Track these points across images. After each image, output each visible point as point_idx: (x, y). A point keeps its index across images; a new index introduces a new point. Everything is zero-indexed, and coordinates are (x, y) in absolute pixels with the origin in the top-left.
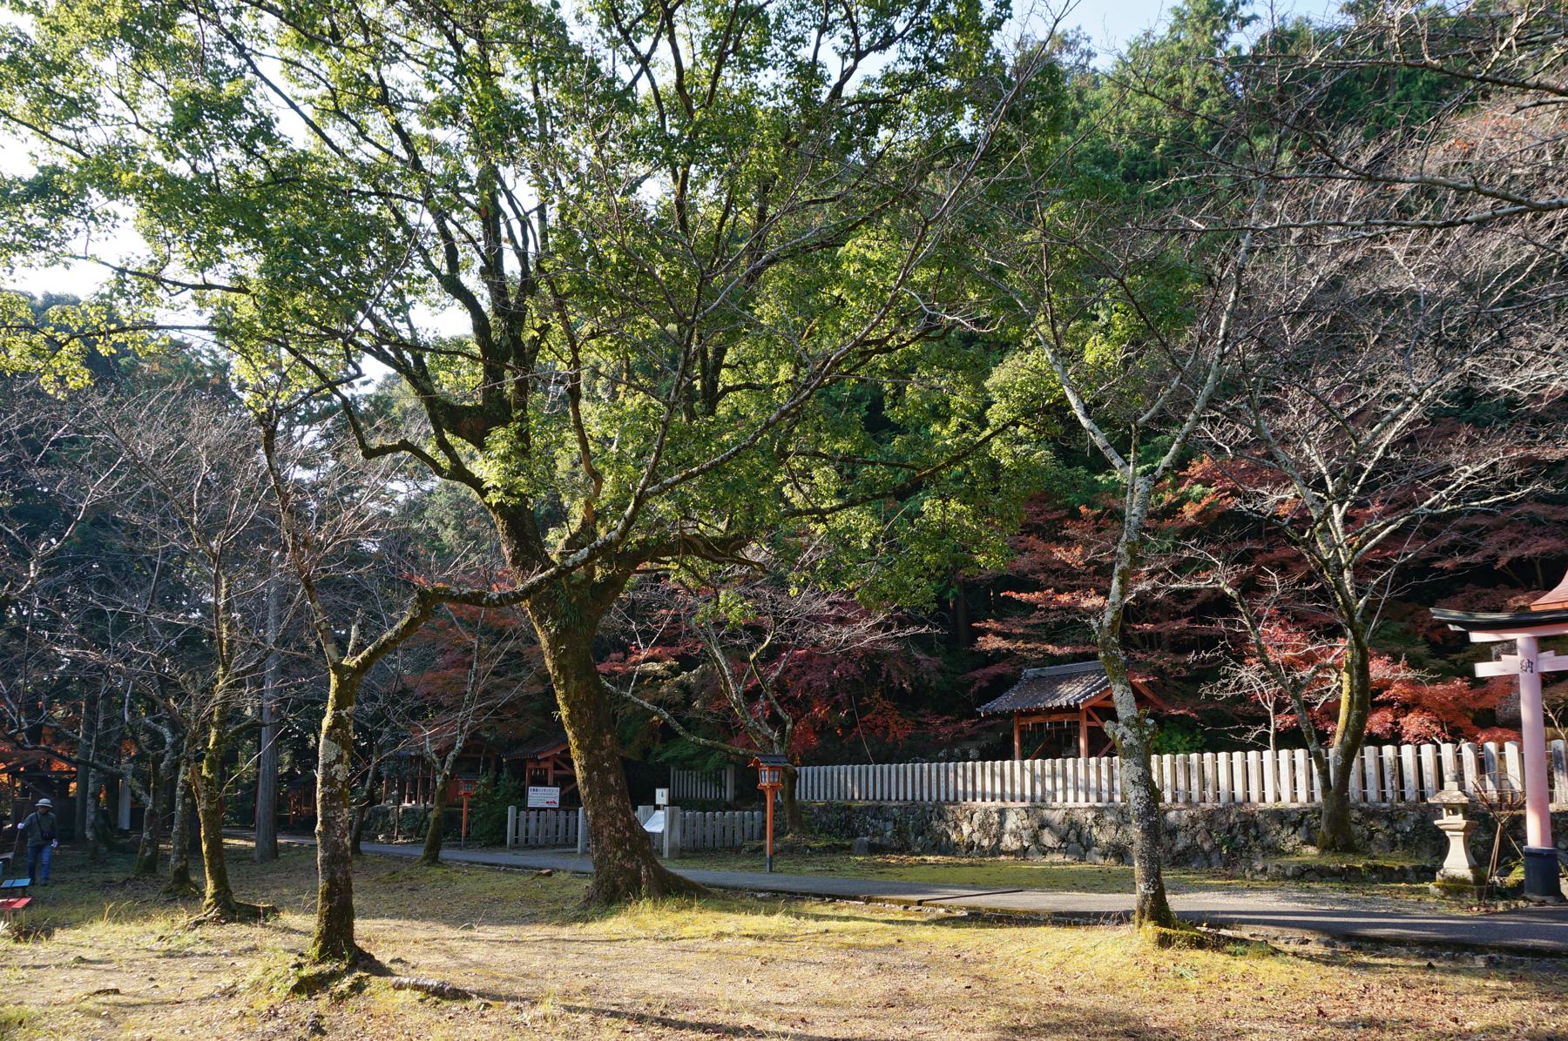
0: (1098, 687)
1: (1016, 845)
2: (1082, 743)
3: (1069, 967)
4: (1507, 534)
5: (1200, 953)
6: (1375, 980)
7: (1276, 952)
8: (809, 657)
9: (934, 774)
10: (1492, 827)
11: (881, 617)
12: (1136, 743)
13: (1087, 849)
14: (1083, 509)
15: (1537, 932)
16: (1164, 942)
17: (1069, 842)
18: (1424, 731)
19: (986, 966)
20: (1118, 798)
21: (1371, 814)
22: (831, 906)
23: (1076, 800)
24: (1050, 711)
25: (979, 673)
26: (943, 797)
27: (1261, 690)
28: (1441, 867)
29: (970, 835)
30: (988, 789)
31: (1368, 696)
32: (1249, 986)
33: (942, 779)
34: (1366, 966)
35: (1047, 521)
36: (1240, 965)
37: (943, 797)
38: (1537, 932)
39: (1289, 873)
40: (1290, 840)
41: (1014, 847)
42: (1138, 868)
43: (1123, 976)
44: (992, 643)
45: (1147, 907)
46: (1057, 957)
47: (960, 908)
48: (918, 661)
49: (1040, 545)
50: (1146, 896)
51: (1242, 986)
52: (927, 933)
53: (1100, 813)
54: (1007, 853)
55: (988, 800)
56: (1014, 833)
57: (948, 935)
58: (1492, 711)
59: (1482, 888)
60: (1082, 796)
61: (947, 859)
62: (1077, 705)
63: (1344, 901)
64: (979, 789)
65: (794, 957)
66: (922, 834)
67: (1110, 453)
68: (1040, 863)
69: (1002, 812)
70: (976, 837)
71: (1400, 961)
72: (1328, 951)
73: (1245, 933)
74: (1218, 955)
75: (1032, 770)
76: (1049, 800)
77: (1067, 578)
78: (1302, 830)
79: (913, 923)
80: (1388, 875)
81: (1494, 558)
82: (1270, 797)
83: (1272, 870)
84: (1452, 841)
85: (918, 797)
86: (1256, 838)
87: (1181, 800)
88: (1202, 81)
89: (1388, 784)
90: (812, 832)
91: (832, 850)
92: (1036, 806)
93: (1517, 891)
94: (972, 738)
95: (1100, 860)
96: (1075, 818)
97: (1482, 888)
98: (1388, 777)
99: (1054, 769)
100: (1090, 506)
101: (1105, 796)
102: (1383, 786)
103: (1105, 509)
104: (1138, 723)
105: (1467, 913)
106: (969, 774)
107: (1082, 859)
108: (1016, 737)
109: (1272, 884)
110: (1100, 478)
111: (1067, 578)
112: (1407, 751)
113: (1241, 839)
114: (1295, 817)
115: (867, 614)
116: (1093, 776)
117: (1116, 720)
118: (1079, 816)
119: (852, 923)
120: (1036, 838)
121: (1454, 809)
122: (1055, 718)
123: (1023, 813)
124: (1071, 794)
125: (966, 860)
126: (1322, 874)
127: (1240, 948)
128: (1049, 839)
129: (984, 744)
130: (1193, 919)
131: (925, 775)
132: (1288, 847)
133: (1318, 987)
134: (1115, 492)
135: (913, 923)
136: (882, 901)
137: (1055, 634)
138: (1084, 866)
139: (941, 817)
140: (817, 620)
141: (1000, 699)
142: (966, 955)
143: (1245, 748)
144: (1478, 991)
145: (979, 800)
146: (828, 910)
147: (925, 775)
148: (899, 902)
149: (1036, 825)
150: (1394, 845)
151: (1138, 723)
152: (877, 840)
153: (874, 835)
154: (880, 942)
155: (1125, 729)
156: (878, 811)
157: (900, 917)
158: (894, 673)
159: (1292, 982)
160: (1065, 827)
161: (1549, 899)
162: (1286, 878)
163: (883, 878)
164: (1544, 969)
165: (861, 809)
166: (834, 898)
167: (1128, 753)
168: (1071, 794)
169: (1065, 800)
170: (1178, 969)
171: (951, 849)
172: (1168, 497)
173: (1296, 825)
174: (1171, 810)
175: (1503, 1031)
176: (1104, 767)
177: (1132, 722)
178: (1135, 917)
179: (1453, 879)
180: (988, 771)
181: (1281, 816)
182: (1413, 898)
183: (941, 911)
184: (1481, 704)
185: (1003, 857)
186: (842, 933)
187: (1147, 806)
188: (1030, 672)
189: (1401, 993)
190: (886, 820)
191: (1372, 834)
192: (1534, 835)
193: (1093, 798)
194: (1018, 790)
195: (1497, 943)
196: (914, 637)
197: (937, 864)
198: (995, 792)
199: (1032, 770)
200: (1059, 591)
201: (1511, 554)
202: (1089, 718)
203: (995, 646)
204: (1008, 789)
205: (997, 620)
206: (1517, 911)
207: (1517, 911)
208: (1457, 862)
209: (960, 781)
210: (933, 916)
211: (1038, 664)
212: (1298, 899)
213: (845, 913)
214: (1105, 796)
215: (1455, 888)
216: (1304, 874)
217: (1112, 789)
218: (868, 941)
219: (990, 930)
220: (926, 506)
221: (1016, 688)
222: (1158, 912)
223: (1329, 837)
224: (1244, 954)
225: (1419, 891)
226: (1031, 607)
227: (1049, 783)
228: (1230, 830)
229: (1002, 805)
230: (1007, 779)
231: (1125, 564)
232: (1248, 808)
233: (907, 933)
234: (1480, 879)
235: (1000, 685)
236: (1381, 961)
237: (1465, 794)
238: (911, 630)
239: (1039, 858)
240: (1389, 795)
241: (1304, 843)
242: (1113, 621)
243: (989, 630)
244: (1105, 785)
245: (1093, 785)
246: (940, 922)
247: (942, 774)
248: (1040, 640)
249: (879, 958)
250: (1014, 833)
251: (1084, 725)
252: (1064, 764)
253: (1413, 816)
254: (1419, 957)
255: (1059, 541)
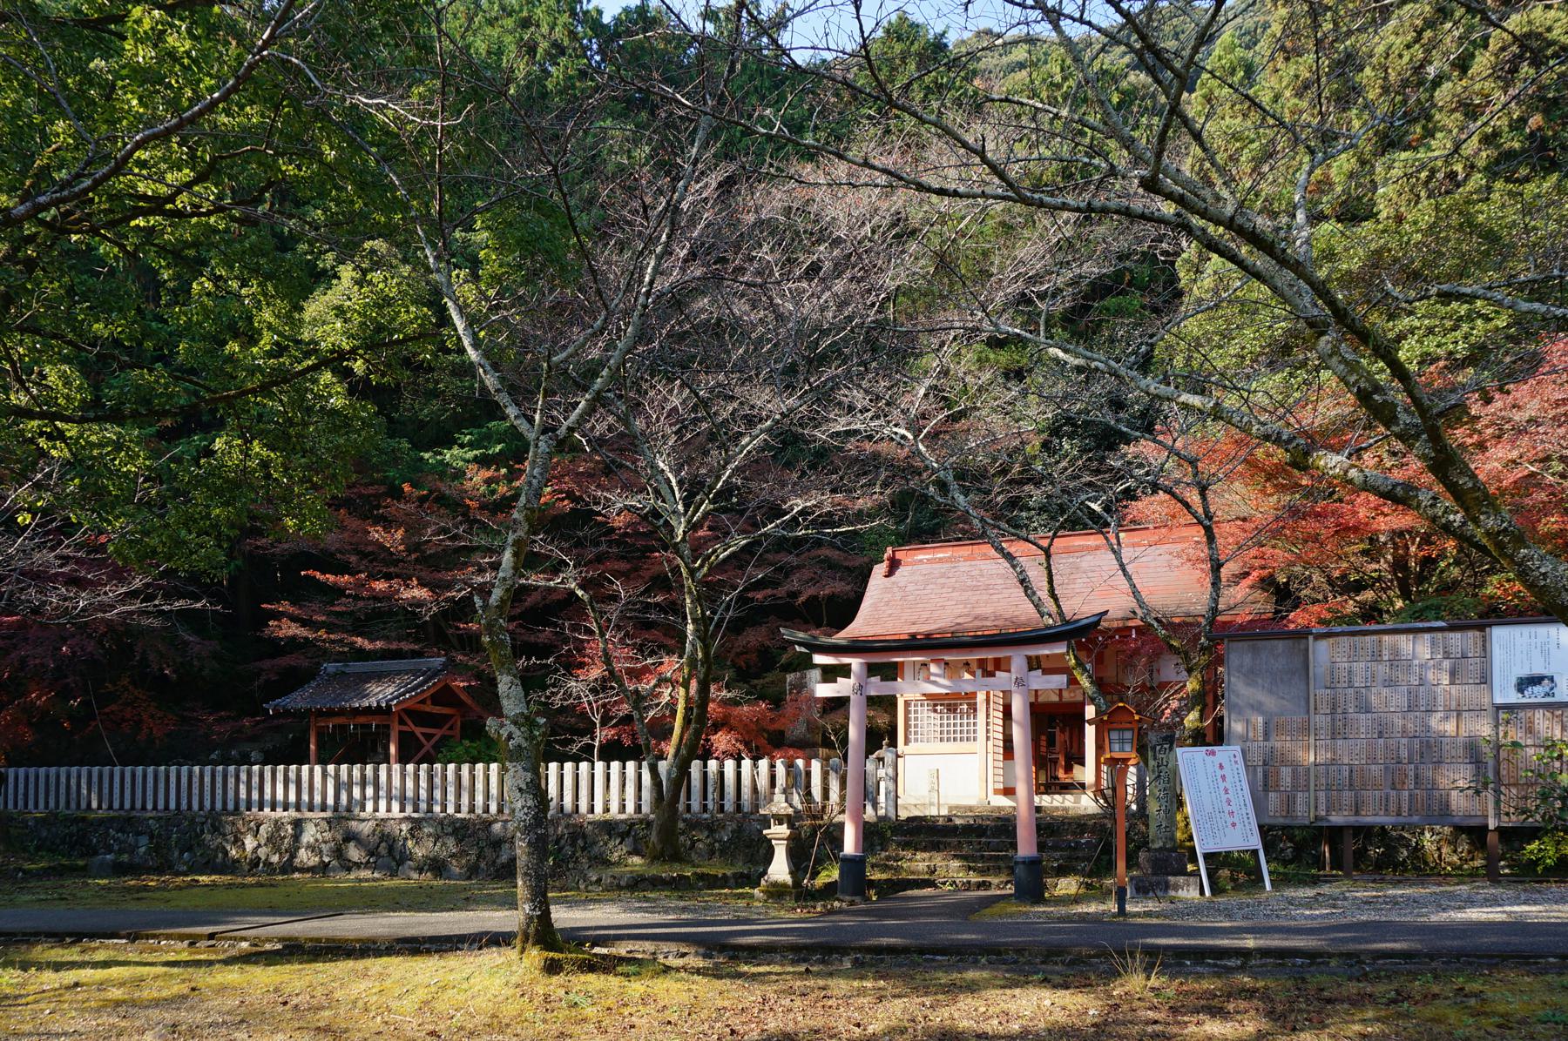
0: (413, 689)
1: (314, 861)
2: (393, 749)
3: (440, 1006)
4: (807, 574)
5: (591, 977)
6: (770, 991)
7: (667, 969)
8: (22, 626)
9: (207, 779)
10: (815, 838)
11: (137, 583)
12: (525, 745)
13: (400, 863)
14: (406, 487)
15: (888, 931)
16: (552, 968)
17: (379, 856)
18: (730, 748)
19: (327, 1013)
20: (437, 809)
21: (694, 825)
22: (77, 949)
23: (389, 810)
24: (356, 712)
25: (266, 664)
26: (219, 806)
27: (590, 703)
28: (765, 873)
29: (255, 850)
30: (280, 796)
31: (698, 714)
32: (651, 1009)
33: (219, 785)
34: (753, 977)
35: (361, 496)
36: (637, 987)
37: (219, 806)
38: (888, 931)
39: (623, 883)
40: (617, 851)
41: (311, 863)
42: (521, 887)
43: (510, 1010)
44: (290, 629)
45: (532, 930)
46: (421, 994)
47: (269, 940)
48: (187, 643)
49: (354, 523)
50: (531, 918)
51: (643, 1010)
52: (232, 975)
53: (416, 824)
54: (302, 870)
55: (279, 810)
56: (311, 848)
57: (263, 976)
58: (782, 733)
59: (798, 893)
60: (396, 806)
61: (227, 879)
62: (389, 707)
63: (684, 909)
64: (267, 796)
65: (27, 1028)
66: (190, 849)
67: (503, 399)
68: (345, 880)
69: (298, 824)
70: (262, 852)
71: (777, 969)
72: (708, 963)
73: (622, 950)
74: (611, 978)
75: (337, 776)
76: (357, 810)
77: (382, 562)
78: (629, 841)
79: (210, 963)
80: (713, 882)
81: (794, 595)
82: (599, 808)
83: (607, 880)
84: (777, 850)
85: (184, 806)
86: (583, 849)
87: (506, 811)
88: (559, 33)
89: (710, 797)
90: (25, 850)
91: (59, 872)
92: (340, 817)
93: (830, 890)
94: (253, 739)
95: (415, 875)
96: (387, 830)
97: (798, 893)
98: (710, 789)
99: (363, 777)
100: (414, 485)
101: (423, 806)
102: (705, 798)
103: (431, 492)
104: (527, 721)
105: (791, 917)
106: (255, 780)
107: (394, 874)
108: (313, 740)
109: (608, 895)
110: (426, 456)
111: (382, 562)
112: (713, 765)
113: (568, 850)
114: (623, 828)
115: (119, 575)
116: (410, 784)
117: (500, 715)
118: (393, 828)
119: (115, 972)
120: (339, 853)
121: (780, 819)
122: (362, 720)
123: (324, 825)
124: (383, 804)
125: (249, 880)
126: (656, 883)
127: (632, 969)
128: (354, 853)
129: (269, 746)
130: (577, 938)
131: (196, 780)
132: (615, 857)
133: (720, 1004)
134: (442, 475)
135: (210, 963)
136: (154, 936)
137: (360, 625)
138: (396, 882)
139: (216, 829)
140: (40, 577)
141: (294, 695)
142: (295, 1001)
143: (577, 760)
144: (862, 992)
145: (267, 810)
146: (72, 954)
147: (196, 780)
148: (181, 938)
149: (339, 837)
150: (712, 853)
151: (527, 721)
152: (125, 857)
153: (121, 851)
154: (165, 993)
155: (513, 728)
156: (128, 823)
157: (184, 956)
158: (152, 657)
159: (693, 1001)
160: (374, 840)
161: (857, 899)
162: (620, 888)
163: (142, 906)
164: (901, 966)
165: (101, 821)
166: (77, 937)
167: (516, 755)
168: (383, 804)
169: (376, 810)
170: (571, 996)
171: (231, 867)
172: (502, 489)
173: (623, 837)
174: (496, 821)
175: (903, 1031)
176: (423, 774)
177: (522, 720)
178: (518, 942)
179: (775, 884)
180: (280, 777)
181: (609, 827)
182: (742, 903)
183: (245, 945)
184: (777, 726)
185: (296, 875)
186: (102, 986)
187: (535, 817)
188: (331, 667)
189: (798, 1003)
190: (138, 834)
191: (693, 843)
192: (850, 846)
193: (409, 808)
194: (318, 799)
195: (858, 944)
196: (182, 613)
197: (214, 885)
198: (291, 799)
199: (337, 776)
200: (373, 577)
201: (811, 591)
202: (402, 722)
203: (290, 633)
204: (305, 797)
205: (293, 604)
206: (831, 912)
207: (831, 912)
208: (779, 869)
209: (243, 788)
210: (233, 952)
211: (341, 658)
212: (640, 909)
213: (100, 956)
214: (423, 806)
215: (777, 892)
216: (637, 885)
217: (431, 798)
218: (146, 994)
219: (319, 966)
220: (219, 444)
221: (313, 684)
222: (543, 934)
223: (659, 847)
224: (637, 974)
225: (740, 896)
226: (339, 592)
227: (356, 792)
228: (557, 842)
229: (298, 815)
230: (305, 785)
231: (520, 533)
232: (576, 820)
233: (202, 977)
234: (797, 883)
235: (294, 680)
236: (761, 969)
237: (791, 806)
238: (179, 604)
239: (342, 875)
240: (710, 806)
241: (629, 853)
242: (502, 600)
243: (283, 614)
244: (423, 794)
245: (410, 794)
246: (246, 959)
247: (219, 779)
248: (344, 630)
249: (169, 1016)
250: (311, 848)
251: (395, 729)
252: (376, 771)
253: (731, 826)
254: (793, 962)
255: (378, 520)
